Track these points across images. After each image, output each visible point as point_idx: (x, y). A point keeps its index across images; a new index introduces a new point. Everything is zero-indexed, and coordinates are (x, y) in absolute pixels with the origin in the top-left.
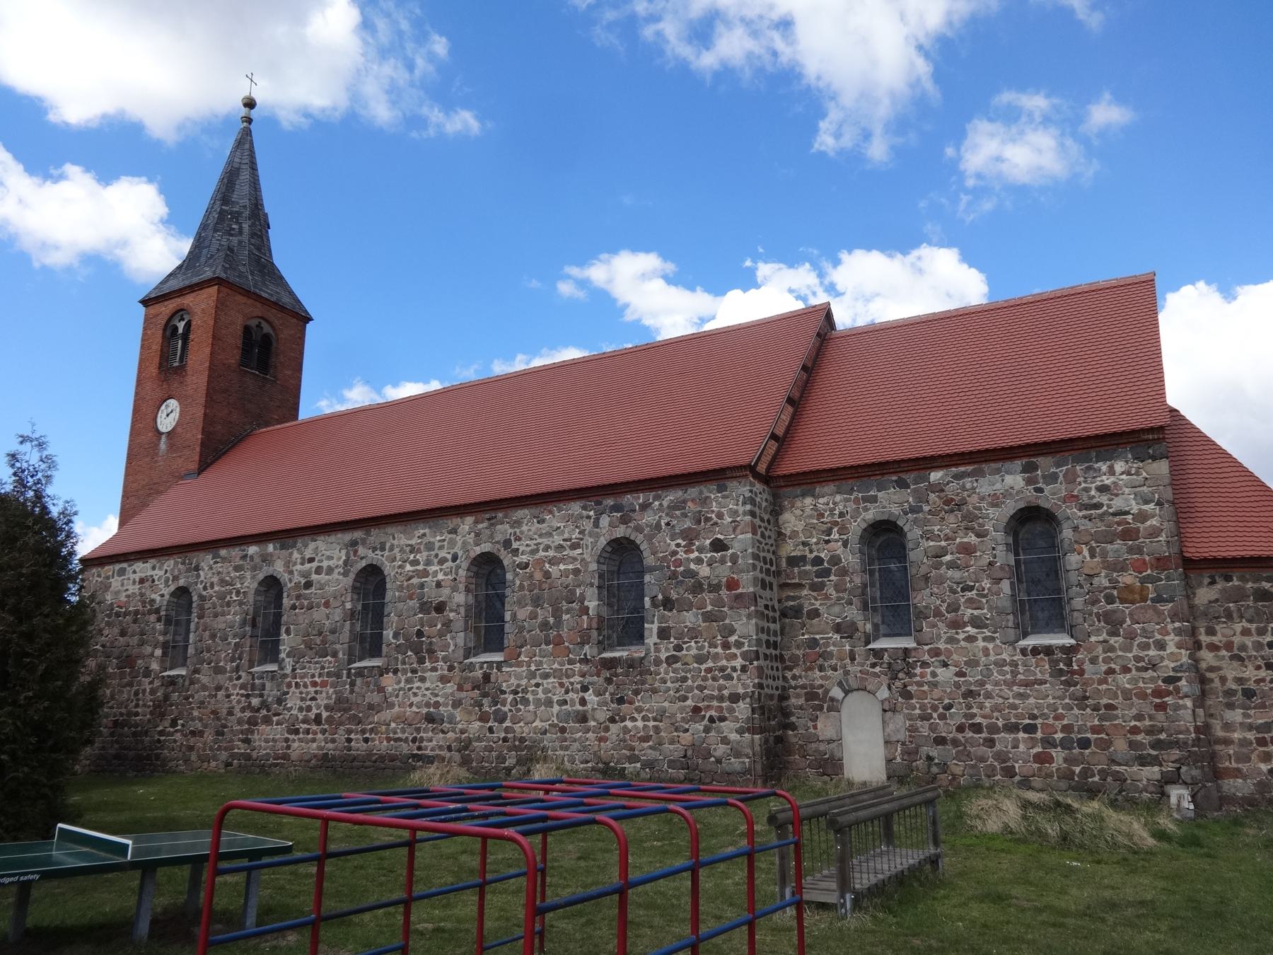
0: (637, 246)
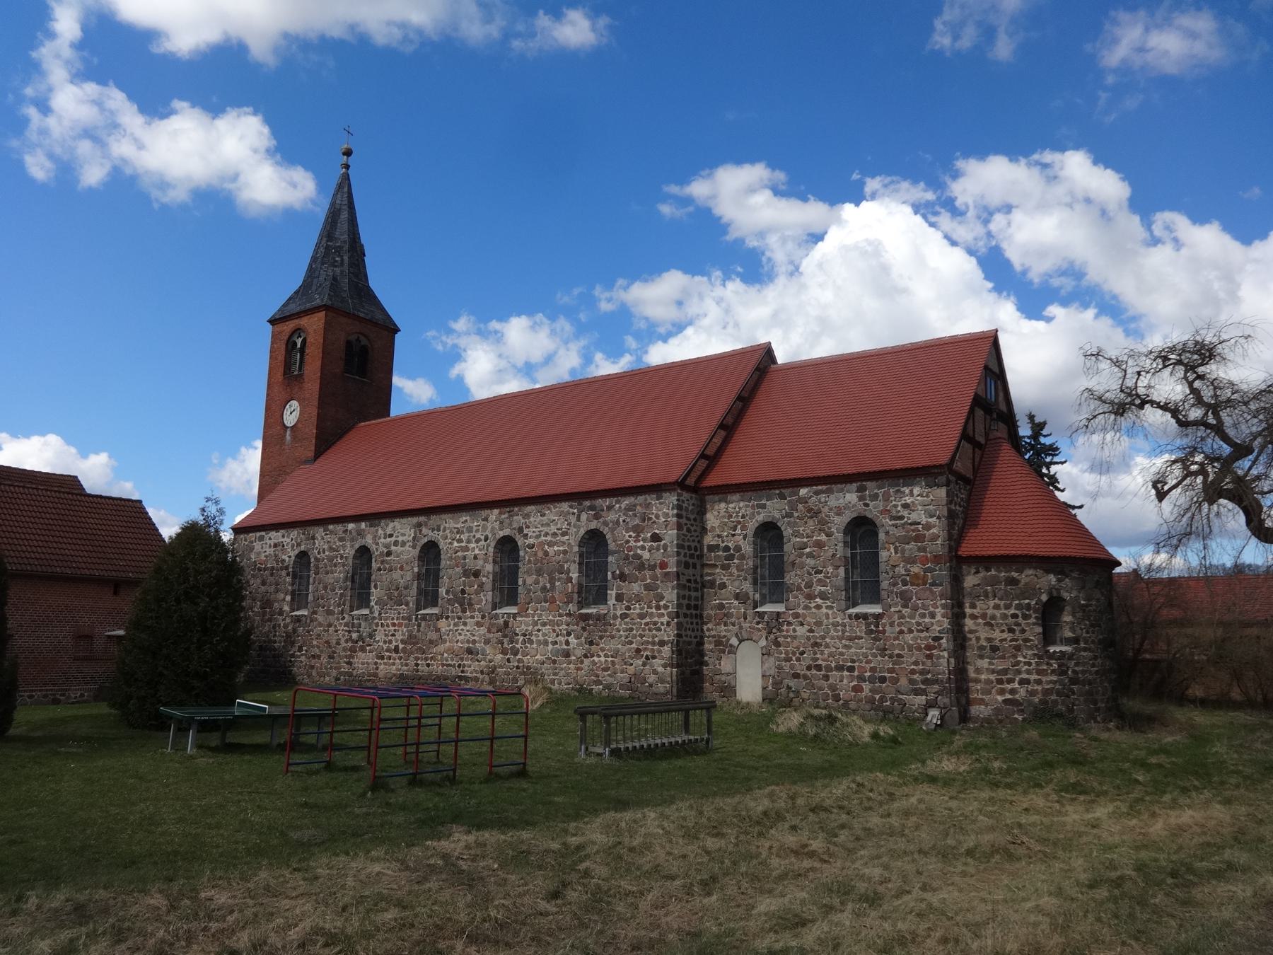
0: (740, 159)
